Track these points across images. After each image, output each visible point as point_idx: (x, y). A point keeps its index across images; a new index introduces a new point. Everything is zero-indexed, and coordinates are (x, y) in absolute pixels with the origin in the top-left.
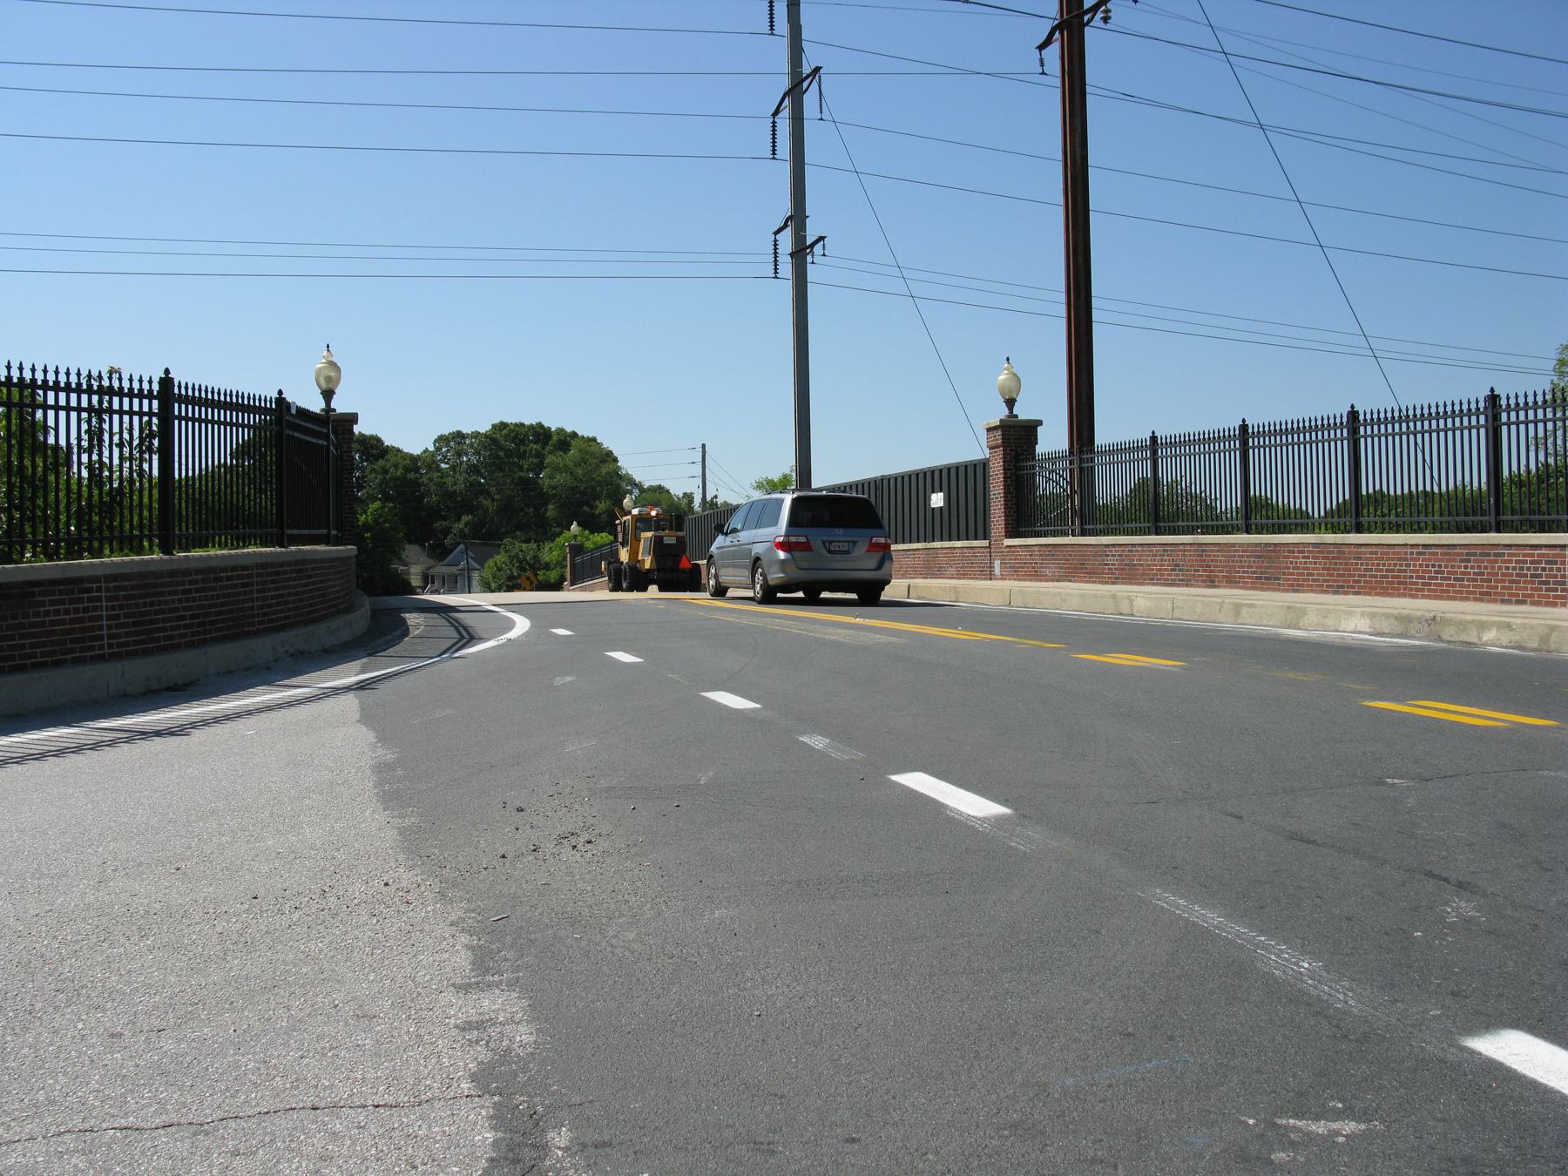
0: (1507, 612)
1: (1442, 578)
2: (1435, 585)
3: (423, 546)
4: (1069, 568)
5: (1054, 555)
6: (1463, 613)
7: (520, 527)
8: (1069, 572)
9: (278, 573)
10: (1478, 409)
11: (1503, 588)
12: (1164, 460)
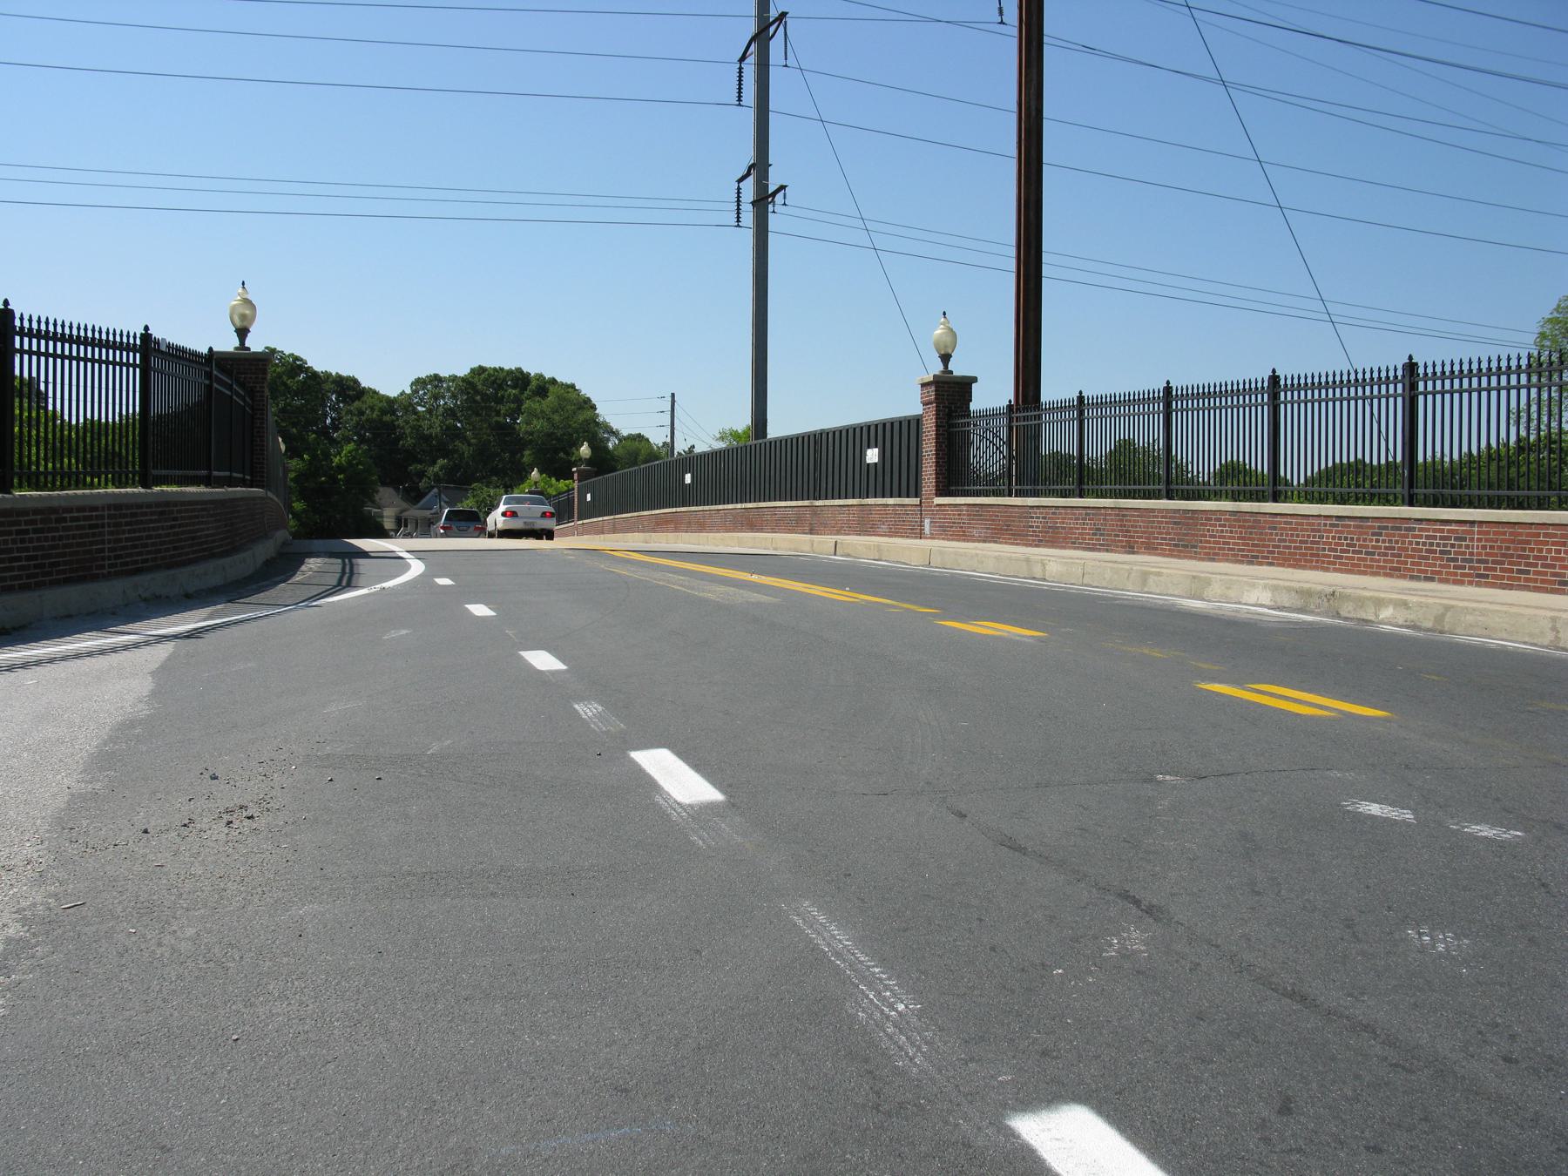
0: (1410, 589)
1: (1354, 552)
2: (1347, 558)
3: (397, 489)
4: (995, 529)
5: (981, 515)
6: (1365, 588)
7: (495, 471)
8: (995, 533)
9: (133, 515)
10: (1396, 377)
11: (1412, 564)
12: (1195, 412)
